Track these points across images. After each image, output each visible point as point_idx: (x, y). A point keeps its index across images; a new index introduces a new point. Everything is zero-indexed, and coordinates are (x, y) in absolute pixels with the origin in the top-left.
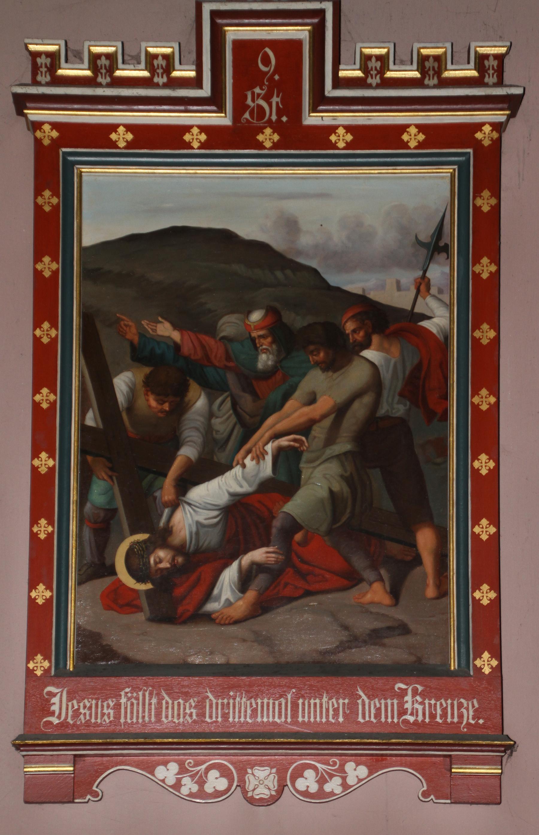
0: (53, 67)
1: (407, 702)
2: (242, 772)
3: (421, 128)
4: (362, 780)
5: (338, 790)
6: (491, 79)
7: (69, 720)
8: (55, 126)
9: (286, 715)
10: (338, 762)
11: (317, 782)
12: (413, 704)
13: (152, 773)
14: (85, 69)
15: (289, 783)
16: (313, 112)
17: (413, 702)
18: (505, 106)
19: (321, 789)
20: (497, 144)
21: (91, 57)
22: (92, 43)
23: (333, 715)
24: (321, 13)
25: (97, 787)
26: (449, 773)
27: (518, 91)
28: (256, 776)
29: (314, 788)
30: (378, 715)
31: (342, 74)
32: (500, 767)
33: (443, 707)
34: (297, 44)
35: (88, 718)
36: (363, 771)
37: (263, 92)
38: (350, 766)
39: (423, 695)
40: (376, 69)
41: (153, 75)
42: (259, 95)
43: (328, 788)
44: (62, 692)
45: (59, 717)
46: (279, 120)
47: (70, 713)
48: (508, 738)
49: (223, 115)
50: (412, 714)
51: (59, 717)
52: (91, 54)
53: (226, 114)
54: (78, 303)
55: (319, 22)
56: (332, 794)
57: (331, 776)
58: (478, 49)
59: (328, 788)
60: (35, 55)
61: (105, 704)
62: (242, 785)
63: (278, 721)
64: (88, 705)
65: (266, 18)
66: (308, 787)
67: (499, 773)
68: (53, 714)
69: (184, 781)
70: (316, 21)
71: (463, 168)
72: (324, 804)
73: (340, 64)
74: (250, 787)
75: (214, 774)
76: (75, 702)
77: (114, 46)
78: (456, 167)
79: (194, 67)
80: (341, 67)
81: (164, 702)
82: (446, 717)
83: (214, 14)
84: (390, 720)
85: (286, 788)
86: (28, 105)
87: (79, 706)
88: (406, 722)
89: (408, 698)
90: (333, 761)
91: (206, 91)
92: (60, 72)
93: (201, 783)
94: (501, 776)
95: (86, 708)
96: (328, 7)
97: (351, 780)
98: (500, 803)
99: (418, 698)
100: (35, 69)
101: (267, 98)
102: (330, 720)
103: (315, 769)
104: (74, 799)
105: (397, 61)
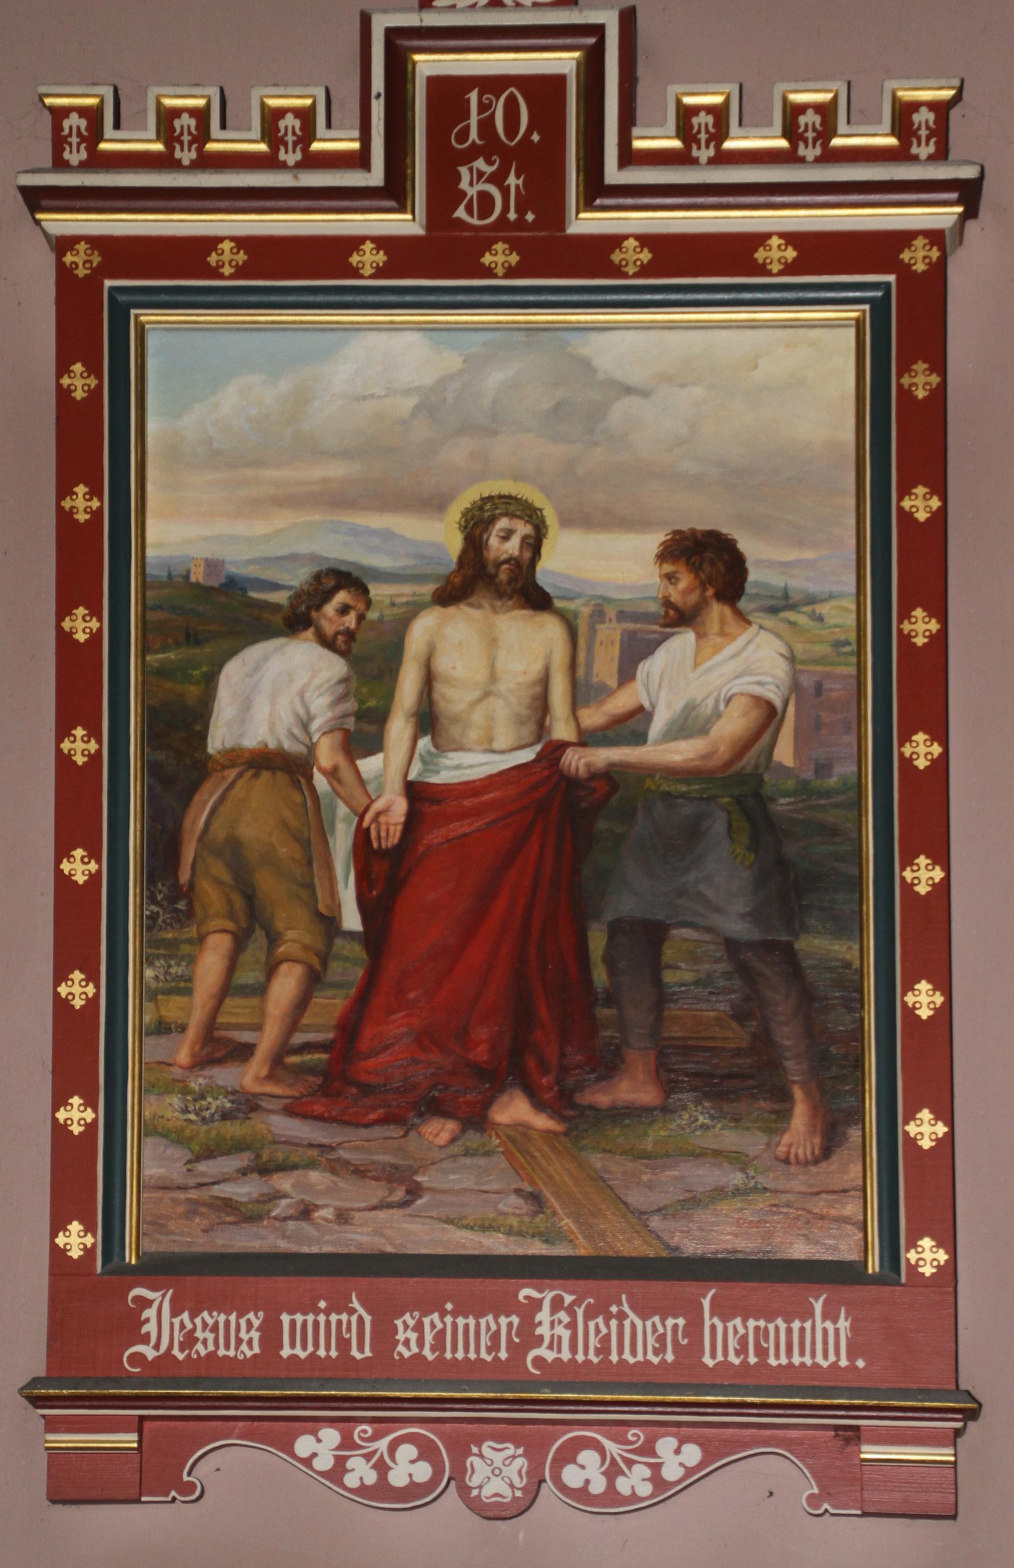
0: (95, 134)
1: (540, 1323)
2: (460, 1451)
4: (311, 1467)
5: (645, 1489)
8: (96, 242)
9: (837, 1353)
10: (641, 1435)
11: (604, 1473)
12: (552, 1326)
14: (669, 138)
16: (585, 211)
17: (552, 1323)
18: (954, 196)
20: (939, 270)
21: (681, 112)
22: (170, 90)
23: (181, 1344)
24: (598, 30)
25: (189, 1474)
27: (969, 173)
28: (512, 1461)
29: (599, 1485)
30: (604, 1349)
31: (638, 144)
32: (951, 1451)
33: (185, 1331)
34: (558, 81)
35: (415, 1349)
37: (489, 170)
38: (666, 1445)
41: (794, 146)
42: (481, 174)
43: (623, 1485)
44: (164, 1296)
47: (178, 1337)
49: (409, 217)
50: (550, 1347)
51: (157, 1347)
52: (162, 109)
53: (413, 213)
55: (596, 43)
56: (634, 1498)
57: (630, 1463)
58: (900, 94)
60: (59, 114)
62: (459, 1474)
63: (631, 1360)
64: (210, 1322)
65: (503, 38)
66: (361, 1479)
68: (145, 1339)
69: (350, 1464)
70: (591, 41)
71: (880, 309)
73: (635, 125)
74: (474, 1481)
75: (407, 1451)
76: (185, 1316)
77: (202, 97)
78: (867, 307)
79: (356, 134)
80: (636, 131)
82: (609, 1352)
83: (392, 34)
85: (543, 1485)
86: (44, 203)
89: (544, 1316)
90: (634, 1435)
91: (376, 176)
93: (382, 1468)
94: (955, 1468)
95: (254, 1329)
97: (671, 1472)
98: (954, 1517)
99: (564, 1316)
100: (59, 142)
101: (498, 179)
102: (173, 1353)
104: (140, 1495)
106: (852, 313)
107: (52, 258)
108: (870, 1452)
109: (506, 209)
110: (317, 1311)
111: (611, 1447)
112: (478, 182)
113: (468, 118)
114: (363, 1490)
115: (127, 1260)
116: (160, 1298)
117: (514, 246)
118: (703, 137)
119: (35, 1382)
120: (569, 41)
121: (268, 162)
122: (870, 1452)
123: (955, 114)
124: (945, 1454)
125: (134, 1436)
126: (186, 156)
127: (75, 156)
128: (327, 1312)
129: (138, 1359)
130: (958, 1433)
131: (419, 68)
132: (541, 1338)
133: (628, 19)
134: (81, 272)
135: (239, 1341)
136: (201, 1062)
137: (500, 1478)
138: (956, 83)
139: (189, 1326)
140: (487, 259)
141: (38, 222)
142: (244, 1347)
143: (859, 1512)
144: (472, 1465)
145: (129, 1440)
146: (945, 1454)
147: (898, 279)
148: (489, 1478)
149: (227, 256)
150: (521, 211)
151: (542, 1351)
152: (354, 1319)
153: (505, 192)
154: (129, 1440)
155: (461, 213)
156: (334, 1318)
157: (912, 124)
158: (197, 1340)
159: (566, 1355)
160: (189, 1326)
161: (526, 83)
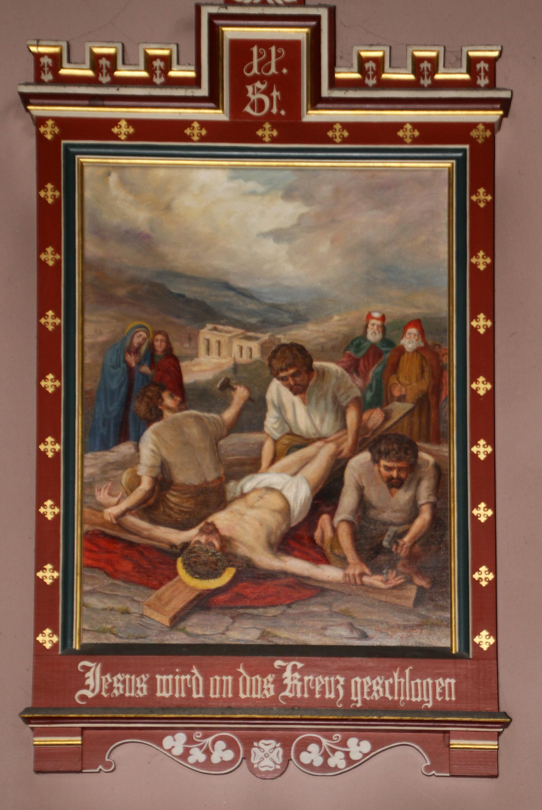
2: (249, 743)
3: (131, 122)
5: (342, 764)
6: (483, 82)
7: (104, 694)
8: (59, 121)
13: (160, 745)
15: (293, 757)
18: (498, 106)
19: (325, 763)
20: (491, 142)
22: (415, 48)
24: (318, 18)
25: (108, 758)
26: (448, 749)
28: (274, 750)
29: (318, 761)
31: (338, 76)
36: (366, 746)
37: (263, 87)
38: (352, 742)
39: (301, 671)
40: (373, 70)
41: (97, 75)
42: (258, 89)
43: (332, 762)
44: (96, 666)
45: (93, 691)
46: (278, 113)
47: (105, 687)
48: (505, 715)
51: (93, 691)
53: (223, 109)
54: (80, 293)
56: (336, 768)
57: (334, 751)
59: (332, 762)
60: (38, 56)
61: (265, 680)
62: (247, 756)
67: (495, 749)
68: (87, 687)
69: (191, 752)
70: (314, 23)
71: (461, 163)
72: (219, 776)
74: (254, 760)
75: (221, 745)
76: (108, 676)
77: (168, 49)
78: (454, 161)
79: (193, 68)
80: (337, 70)
81: (241, 679)
83: (212, 17)
84: (224, 696)
85: (291, 762)
86: (32, 101)
87: (113, 680)
88: (285, 698)
89: (288, 674)
91: (204, 91)
92: (63, 72)
93: (208, 752)
96: (324, 13)
97: (355, 755)
98: (496, 776)
100: (39, 69)
101: (268, 92)
103: (319, 743)
104: (82, 769)
105: (447, 64)
106: (447, 164)
107: (34, 129)
108: (456, 743)
109: (271, 107)
110: (175, 674)
111: (325, 742)
112: (257, 92)
113: (251, 59)
114: (197, 764)
115: (74, 647)
116: (94, 667)
117: (273, 127)
118: (371, 73)
119: (27, 710)
120: (302, 23)
121: (98, 84)
122: (456, 743)
123: (498, 65)
124: (491, 745)
125: (79, 738)
126: (158, 80)
127: (47, 77)
128: (180, 674)
129: (83, 697)
130: (499, 734)
131: (225, 34)
132: (286, 685)
133: (332, 12)
134: (49, 137)
135: (136, 688)
136: (229, 563)
137: (268, 758)
138: (500, 48)
139: (110, 680)
140: (260, 133)
141: (28, 111)
142: (139, 692)
143: (448, 775)
144: (254, 751)
145: (77, 740)
146: (491, 745)
147: (471, 149)
148: (263, 758)
149: (123, 130)
150: (279, 109)
151: (287, 693)
152: (194, 678)
153: (271, 99)
154: (77, 740)
155: (248, 109)
156: (183, 677)
157: (420, 68)
158: (114, 688)
159: (299, 695)
160: (110, 680)
161: (279, 44)
